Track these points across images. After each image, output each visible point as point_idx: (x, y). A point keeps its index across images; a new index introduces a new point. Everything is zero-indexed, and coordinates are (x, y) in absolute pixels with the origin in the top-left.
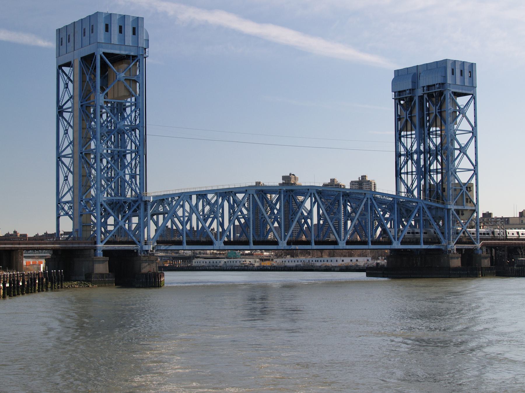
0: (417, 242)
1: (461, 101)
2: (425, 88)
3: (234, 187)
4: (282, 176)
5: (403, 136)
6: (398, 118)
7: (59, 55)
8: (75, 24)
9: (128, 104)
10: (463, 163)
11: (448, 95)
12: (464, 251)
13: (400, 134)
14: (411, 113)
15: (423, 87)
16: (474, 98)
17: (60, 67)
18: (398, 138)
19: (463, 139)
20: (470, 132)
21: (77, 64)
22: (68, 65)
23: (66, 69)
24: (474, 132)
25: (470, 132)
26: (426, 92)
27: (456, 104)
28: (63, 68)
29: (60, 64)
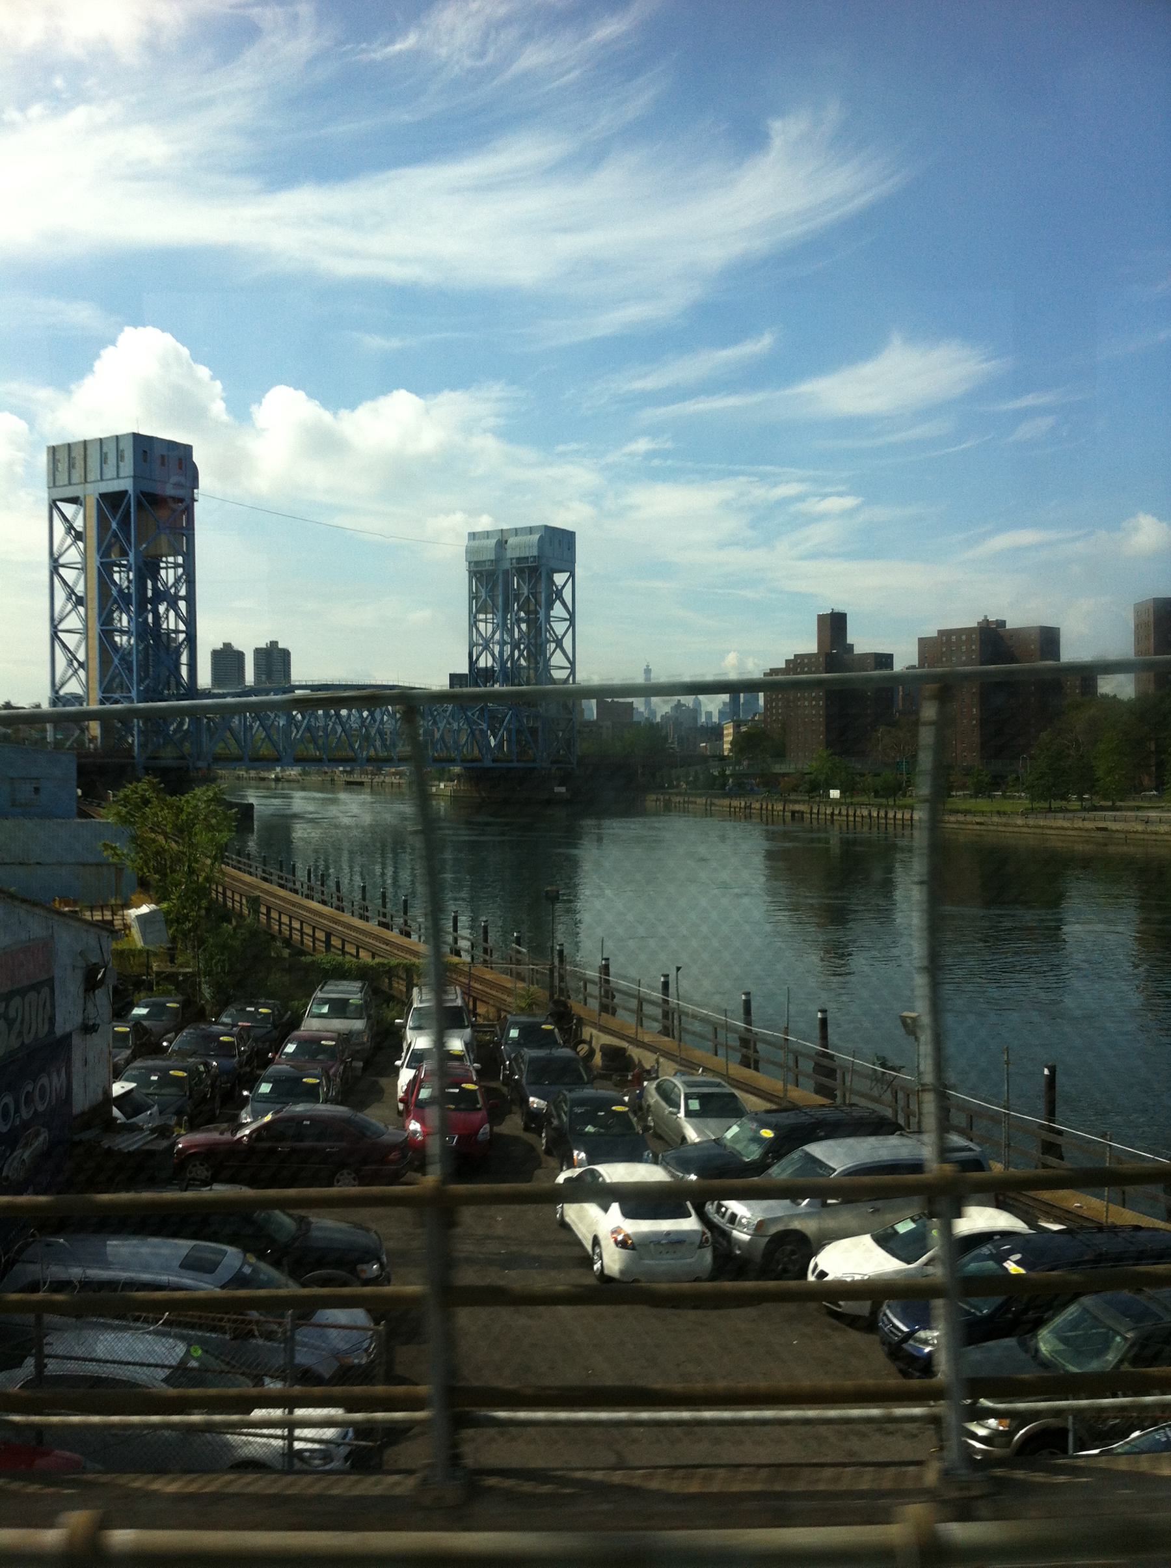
0: (512, 761)
1: (559, 578)
2: (514, 561)
3: (338, 683)
4: (450, 674)
5: (481, 621)
6: (473, 597)
7: (53, 483)
8: (89, 447)
9: (163, 565)
10: (558, 659)
11: (544, 571)
12: (446, 778)
13: (475, 617)
14: (492, 590)
15: (512, 559)
16: (572, 575)
17: (54, 501)
18: (473, 623)
19: (560, 628)
20: (63, 566)
21: (92, 503)
22: (74, 500)
23: (68, 509)
24: (572, 620)
25: (63, 566)
26: (515, 565)
27: (553, 583)
28: (59, 503)
29: (56, 497)
